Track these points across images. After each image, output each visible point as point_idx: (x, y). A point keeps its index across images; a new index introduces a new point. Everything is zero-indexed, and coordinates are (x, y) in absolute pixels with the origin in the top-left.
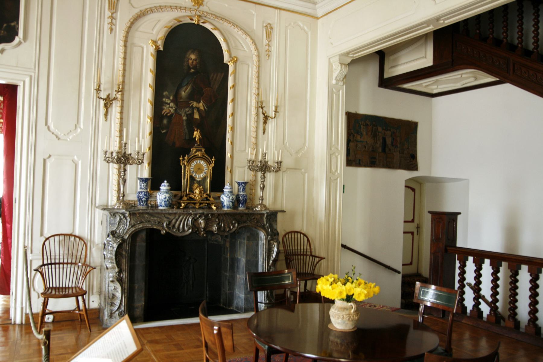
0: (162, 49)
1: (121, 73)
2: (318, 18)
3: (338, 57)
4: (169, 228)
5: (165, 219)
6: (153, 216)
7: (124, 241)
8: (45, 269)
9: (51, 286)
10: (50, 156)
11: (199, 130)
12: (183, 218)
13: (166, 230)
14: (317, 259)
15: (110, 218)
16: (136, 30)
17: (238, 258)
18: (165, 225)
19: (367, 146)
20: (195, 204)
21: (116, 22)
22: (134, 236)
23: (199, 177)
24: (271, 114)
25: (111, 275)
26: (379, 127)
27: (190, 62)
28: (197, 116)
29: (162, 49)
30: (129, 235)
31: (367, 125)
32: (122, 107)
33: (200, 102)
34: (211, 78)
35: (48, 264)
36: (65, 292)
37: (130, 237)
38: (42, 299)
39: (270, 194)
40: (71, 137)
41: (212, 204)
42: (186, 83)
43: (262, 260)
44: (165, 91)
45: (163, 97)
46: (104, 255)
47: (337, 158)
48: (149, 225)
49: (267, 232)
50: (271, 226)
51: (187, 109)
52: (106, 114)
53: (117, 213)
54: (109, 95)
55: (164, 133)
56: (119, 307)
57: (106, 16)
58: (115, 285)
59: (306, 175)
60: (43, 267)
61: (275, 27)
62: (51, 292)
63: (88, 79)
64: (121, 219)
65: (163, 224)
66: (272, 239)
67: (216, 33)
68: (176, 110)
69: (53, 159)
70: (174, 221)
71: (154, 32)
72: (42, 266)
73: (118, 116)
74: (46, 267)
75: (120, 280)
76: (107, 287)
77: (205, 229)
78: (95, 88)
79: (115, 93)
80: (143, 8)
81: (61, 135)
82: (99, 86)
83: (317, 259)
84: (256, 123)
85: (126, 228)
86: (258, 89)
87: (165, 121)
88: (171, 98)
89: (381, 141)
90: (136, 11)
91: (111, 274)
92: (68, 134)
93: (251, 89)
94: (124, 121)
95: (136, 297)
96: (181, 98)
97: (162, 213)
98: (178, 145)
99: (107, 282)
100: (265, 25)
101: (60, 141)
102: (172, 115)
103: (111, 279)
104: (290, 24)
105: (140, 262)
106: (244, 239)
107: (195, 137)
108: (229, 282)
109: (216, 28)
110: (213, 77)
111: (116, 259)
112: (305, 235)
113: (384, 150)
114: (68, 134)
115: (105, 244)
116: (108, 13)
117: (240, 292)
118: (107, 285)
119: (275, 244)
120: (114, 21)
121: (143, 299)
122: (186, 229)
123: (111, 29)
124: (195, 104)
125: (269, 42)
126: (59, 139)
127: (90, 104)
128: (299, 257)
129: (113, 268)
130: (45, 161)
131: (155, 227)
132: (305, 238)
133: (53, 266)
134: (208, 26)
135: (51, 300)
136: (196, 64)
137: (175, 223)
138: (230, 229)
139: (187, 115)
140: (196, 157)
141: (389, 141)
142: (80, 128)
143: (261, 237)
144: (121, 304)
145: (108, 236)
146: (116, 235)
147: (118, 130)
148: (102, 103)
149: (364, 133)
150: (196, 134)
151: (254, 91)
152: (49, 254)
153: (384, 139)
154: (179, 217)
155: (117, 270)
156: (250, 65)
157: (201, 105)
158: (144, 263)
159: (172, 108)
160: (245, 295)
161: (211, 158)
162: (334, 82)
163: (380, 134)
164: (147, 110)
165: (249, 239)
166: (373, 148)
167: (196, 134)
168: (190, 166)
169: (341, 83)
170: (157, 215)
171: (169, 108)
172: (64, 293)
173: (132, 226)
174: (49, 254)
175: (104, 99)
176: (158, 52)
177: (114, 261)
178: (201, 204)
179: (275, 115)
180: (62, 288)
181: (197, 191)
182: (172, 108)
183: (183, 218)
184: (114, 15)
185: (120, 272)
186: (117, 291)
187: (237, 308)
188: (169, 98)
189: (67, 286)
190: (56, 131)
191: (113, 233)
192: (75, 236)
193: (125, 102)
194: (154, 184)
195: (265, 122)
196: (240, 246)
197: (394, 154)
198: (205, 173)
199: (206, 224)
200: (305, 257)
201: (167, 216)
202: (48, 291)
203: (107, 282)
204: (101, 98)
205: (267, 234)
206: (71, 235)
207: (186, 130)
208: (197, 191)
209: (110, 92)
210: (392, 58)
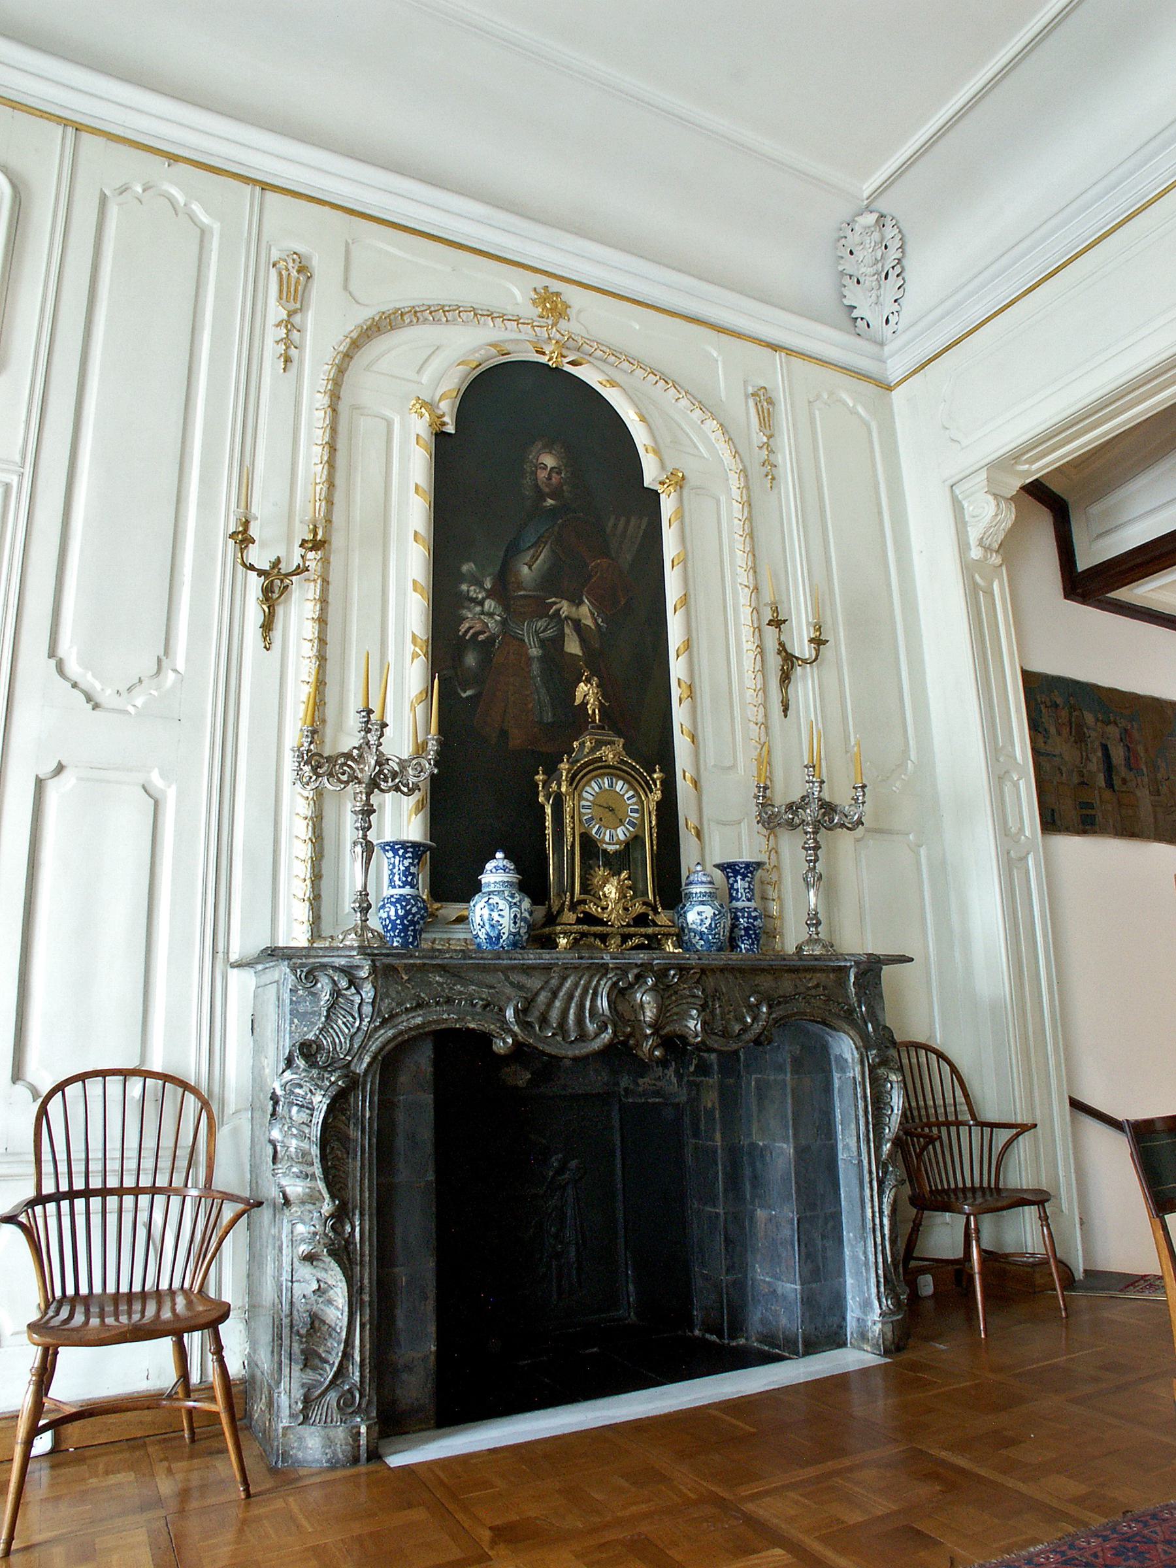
0: (451, 429)
1: (321, 489)
2: (889, 388)
3: (983, 475)
4: (526, 1025)
5: (509, 990)
6: (465, 982)
7: (353, 1083)
8: (48, 1217)
9: (70, 1291)
10: (60, 769)
11: (595, 681)
12: (576, 985)
13: (514, 1035)
14: (1003, 1136)
15: (292, 1022)
16: (368, 368)
17: (753, 1145)
18: (510, 1014)
19: (1064, 769)
20: (603, 938)
21: (303, 339)
22: (389, 1062)
23: (612, 838)
24: (802, 648)
25: (301, 1229)
26: (1085, 713)
27: (542, 475)
28: (573, 647)
29: (451, 429)
30: (374, 1058)
31: (1057, 706)
32: (324, 601)
33: (581, 603)
34: (608, 530)
35: (57, 1197)
36: (143, 1312)
37: (377, 1067)
38: (32, 1355)
39: (823, 908)
40: (139, 702)
41: (667, 936)
42: (533, 540)
43: (853, 1142)
44: (468, 560)
45: (461, 578)
46: (272, 1143)
47: (1016, 785)
48: (448, 1017)
49: (864, 1035)
50: (873, 1016)
51: (541, 624)
52: (267, 626)
53: (324, 966)
54: (278, 560)
55: (470, 697)
56: (341, 1372)
57: (272, 319)
58: (321, 1275)
59: (923, 851)
60: (39, 1209)
61: (780, 397)
62: (65, 1322)
63: (206, 504)
64: (336, 993)
65: (502, 1010)
66: (885, 1062)
67: (612, 396)
68: (504, 622)
69: (68, 780)
70: (543, 998)
71: (425, 379)
72: (31, 1204)
73: (311, 630)
74: (51, 1207)
75: (342, 1252)
76: (285, 1284)
77: (656, 1026)
78: (231, 530)
79: (298, 551)
80: (388, 307)
81: (105, 695)
82: (246, 524)
83: (1003, 1136)
84: (759, 675)
85: (356, 1029)
86: (754, 569)
87: (471, 660)
88: (488, 585)
89: (1100, 754)
90: (363, 315)
91: (302, 1228)
92: (129, 690)
93: (734, 574)
94: (332, 651)
95: (400, 1324)
96: (520, 586)
97: (495, 969)
98: (517, 739)
99: (286, 1260)
100: (750, 390)
101: (97, 713)
102: (491, 641)
103: (304, 1248)
104: (818, 397)
105: (416, 1173)
106: (780, 1068)
107: (584, 704)
108: (726, 1240)
109: (613, 384)
110: (615, 526)
111: (323, 1158)
112: (941, 1056)
113: (1110, 784)
114: (129, 690)
115: (275, 1099)
116: (276, 312)
117: (776, 1277)
118: (286, 1276)
119: (893, 1078)
120: (295, 335)
121: (432, 1329)
122: (591, 1027)
123: (288, 360)
124: (565, 608)
125: (770, 437)
126: (96, 706)
127: (213, 592)
128: (944, 1129)
129: (312, 1198)
130: (40, 784)
131: (472, 1026)
132: (943, 1064)
133: (96, 1202)
134: (588, 374)
135: (66, 1355)
136: (560, 485)
137: (550, 1005)
138: (745, 1029)
139: (542, 643)
140: (598, 768)
141: (1118, 754)
142: (175, 670)
143: (840, 1059)
144: (346, 1355)
145: (289, 1062)
146: (321, 1059)
147: (312, 679)
148: (255, 583)
149: (1053, 730)
150: (586, 692)
151: (744, 577)
152: (61, 1156)
153: (1105, 748)
154: (564, 979)
155: (327, 1207)
156: (723, 499)
157: (585, 612)
158: (431, 1177)
159: (491, 615)
160: (802, 1284)
161: (651, 771)
162: (976, 553)
163: (1093, 734)
164: (411, 614)
165: (798, 1065)
166: (1081, 774)
167: (586, 692)
168: (581, 798)
169: (996, 559)
170: (476, 976)
171: (482, 616)
172: (124, 1319)
173: (384, 1022)
174: (61, 1156)
175: (261, 573)
176: (440, 437)
177: (317, 1169)
178: (625, 938)
179: (818, 651)
180: (130, 1295)
181: (611, 890)
182: (491, 615)
183: (576, 985)
184: (297, 319)
185: (340, 1215)
186: (330, 1302)
187: (769, 1338)
188: (480, 585)
189: (137, 1288)
190: (89, 680)
191: (308, 1051)
192: (147, 1074)
193: (330, 666)
194: (446, 869)
195: (785, 678)
196: (761, 1097)
197: (1139, 794)
198: (633, 825)
199: (662, 1009)
200: (953, 1129)
201: (515, 978)
202: (57, 1313)
203: (286, 1260)
204: (251, 568)
205: (865, 1044)
206: (135, 1072)
207: (543, 691)
208: (611, 890)
209: (281, 553)
210: (1095, 509)
